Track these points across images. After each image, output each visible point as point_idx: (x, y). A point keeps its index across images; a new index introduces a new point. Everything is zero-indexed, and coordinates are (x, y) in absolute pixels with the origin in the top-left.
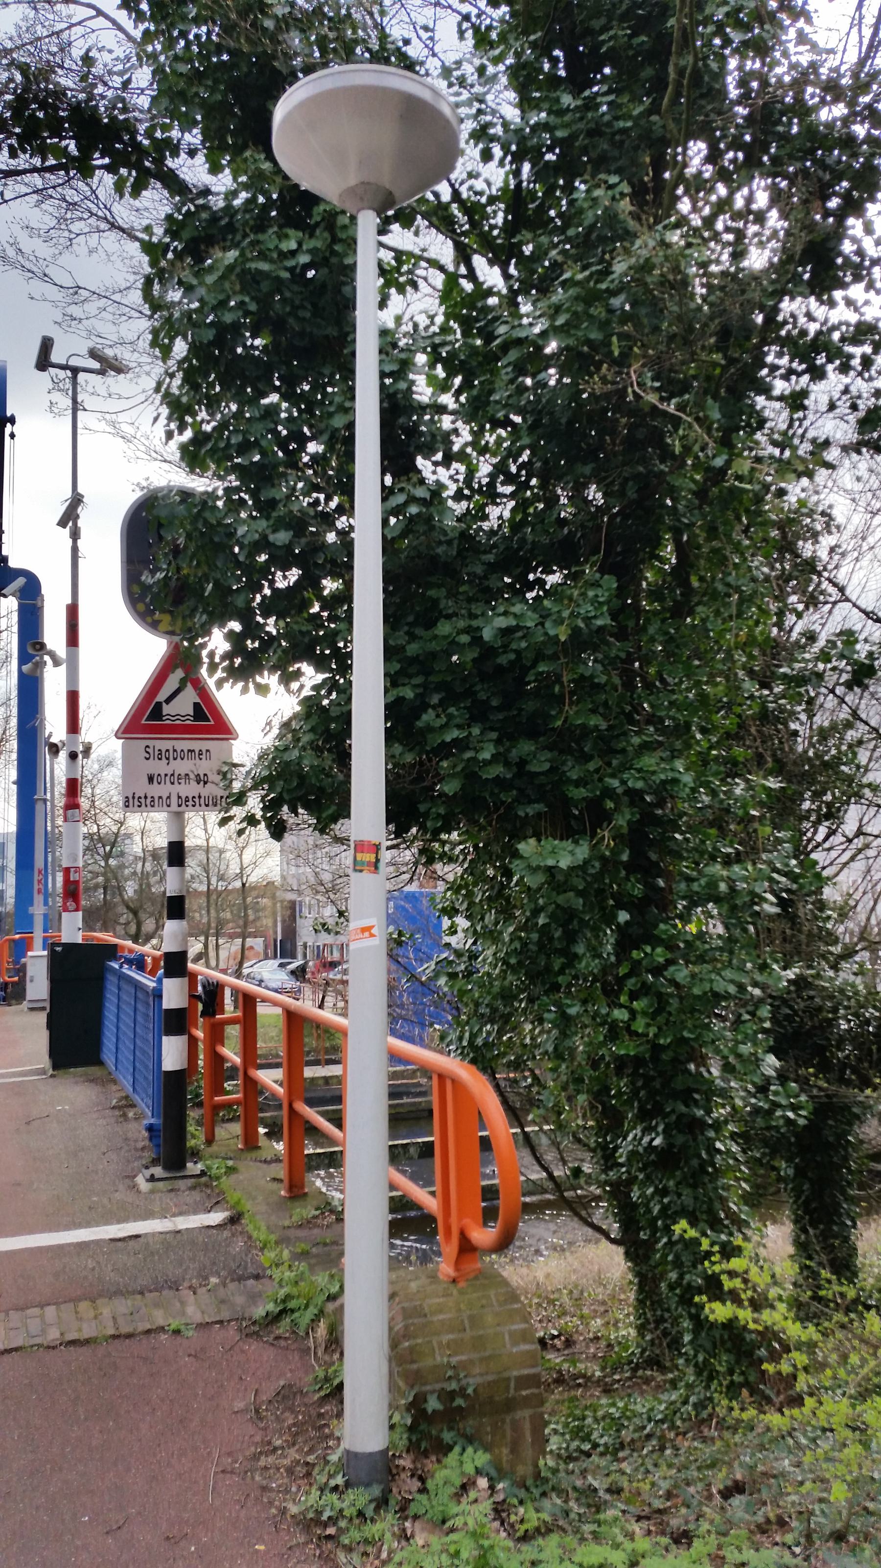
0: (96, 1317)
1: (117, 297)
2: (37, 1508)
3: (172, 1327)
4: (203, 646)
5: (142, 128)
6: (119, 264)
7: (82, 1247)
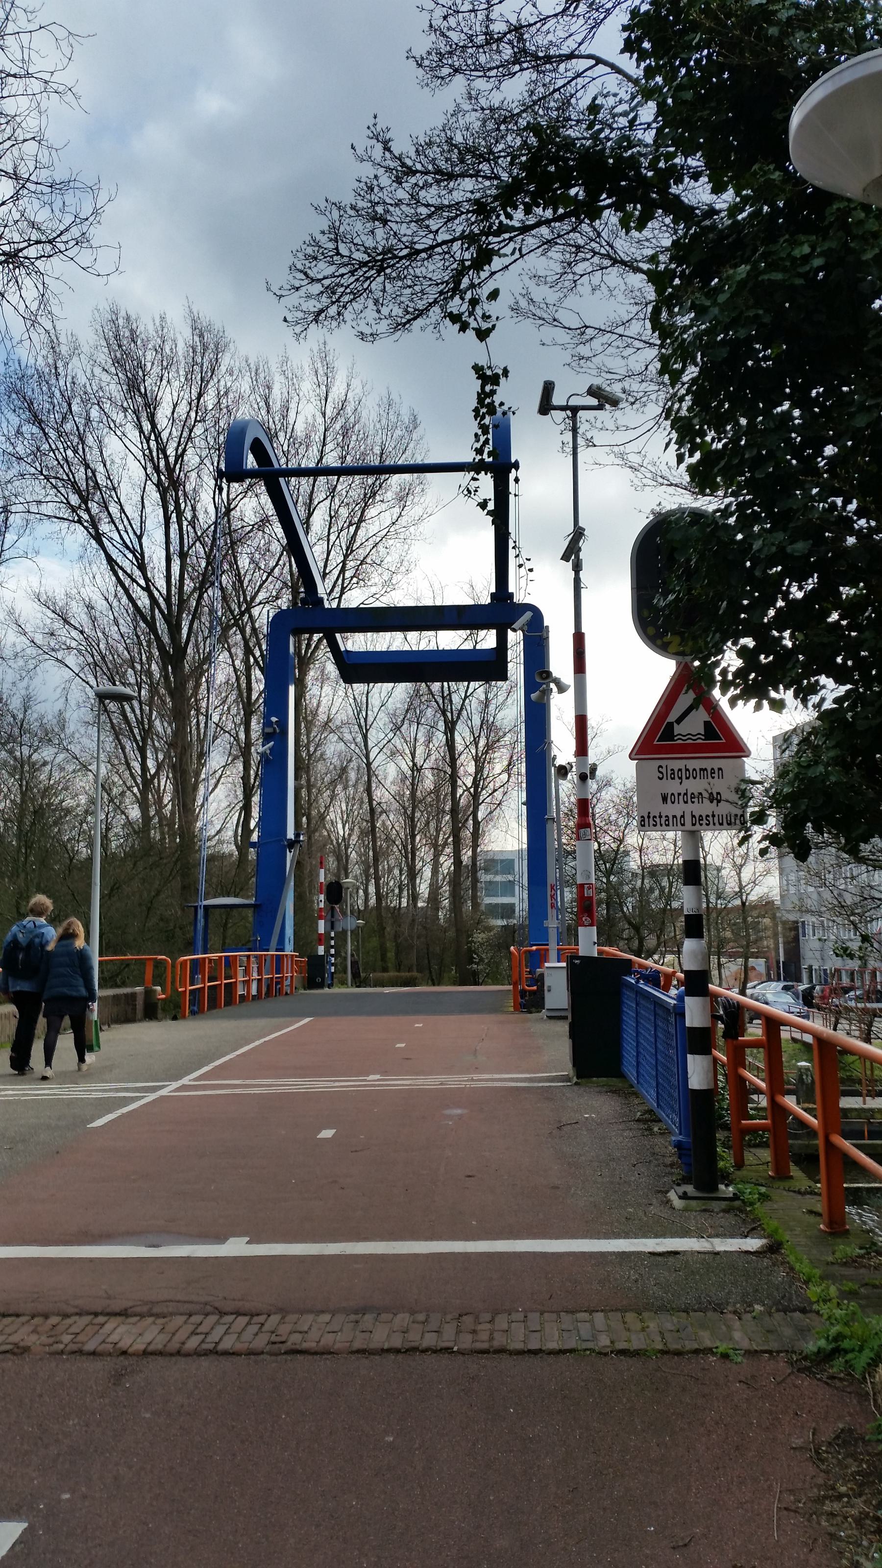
0: (643, 1329)
1: (620, 330)
2: (605, 1509)
3: (720, 1350)
4: (717, 664)
5: (645, 162)
6: (621, 298)
7: (623, 1256)
